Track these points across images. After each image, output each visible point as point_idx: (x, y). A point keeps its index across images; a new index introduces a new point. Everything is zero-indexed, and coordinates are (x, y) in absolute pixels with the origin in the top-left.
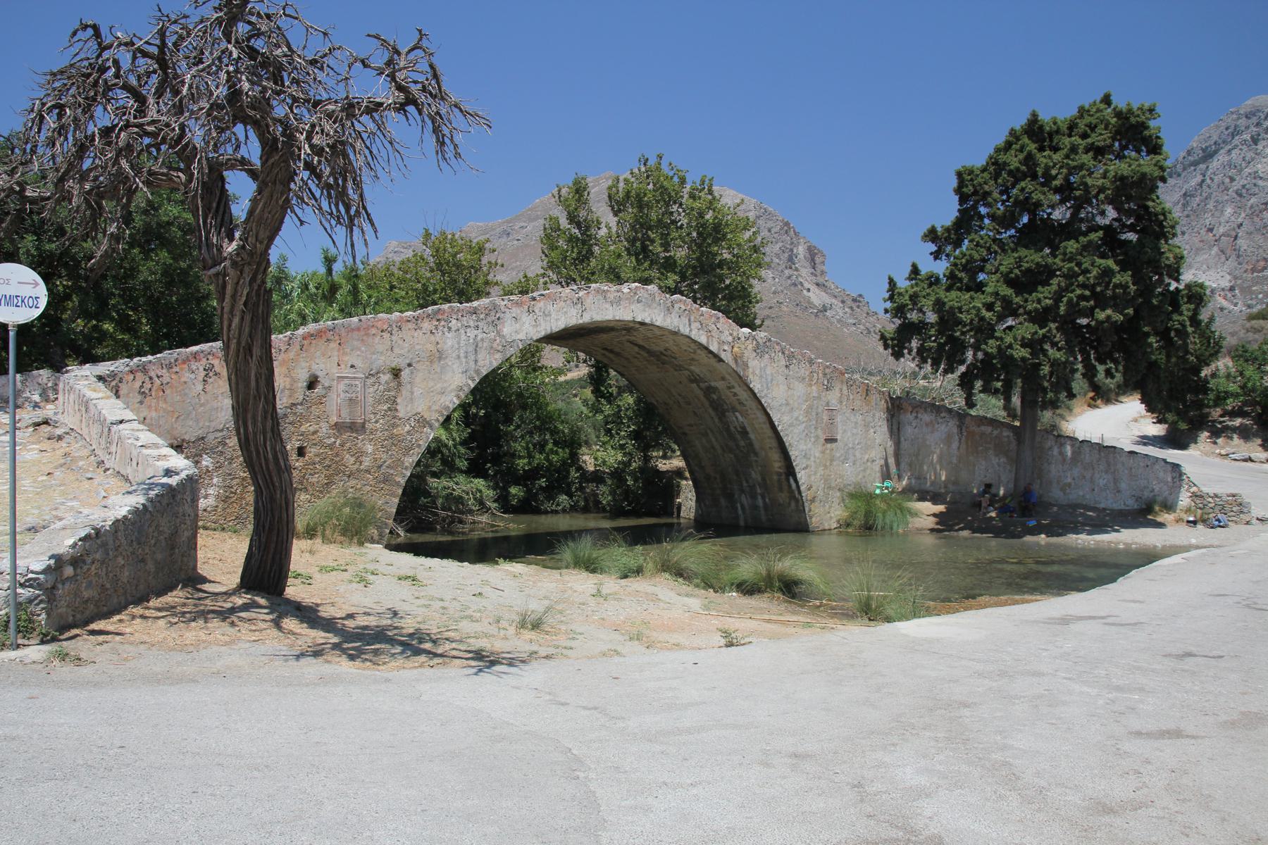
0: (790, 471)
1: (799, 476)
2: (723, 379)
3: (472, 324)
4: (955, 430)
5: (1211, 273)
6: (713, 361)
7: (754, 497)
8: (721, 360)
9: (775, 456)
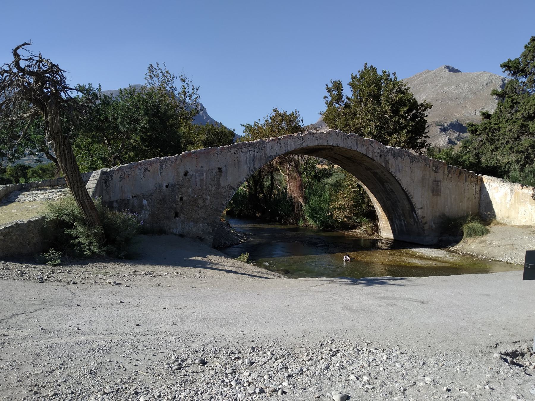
0: (413, 209)
1: (417, 212)
2: (378, 168)
3: (252, 149)
4: (509, 191)
5: (435, 154)
6: (371, 160)
7: (400, 221)
8: (374, 160)
9: (406, 203)
